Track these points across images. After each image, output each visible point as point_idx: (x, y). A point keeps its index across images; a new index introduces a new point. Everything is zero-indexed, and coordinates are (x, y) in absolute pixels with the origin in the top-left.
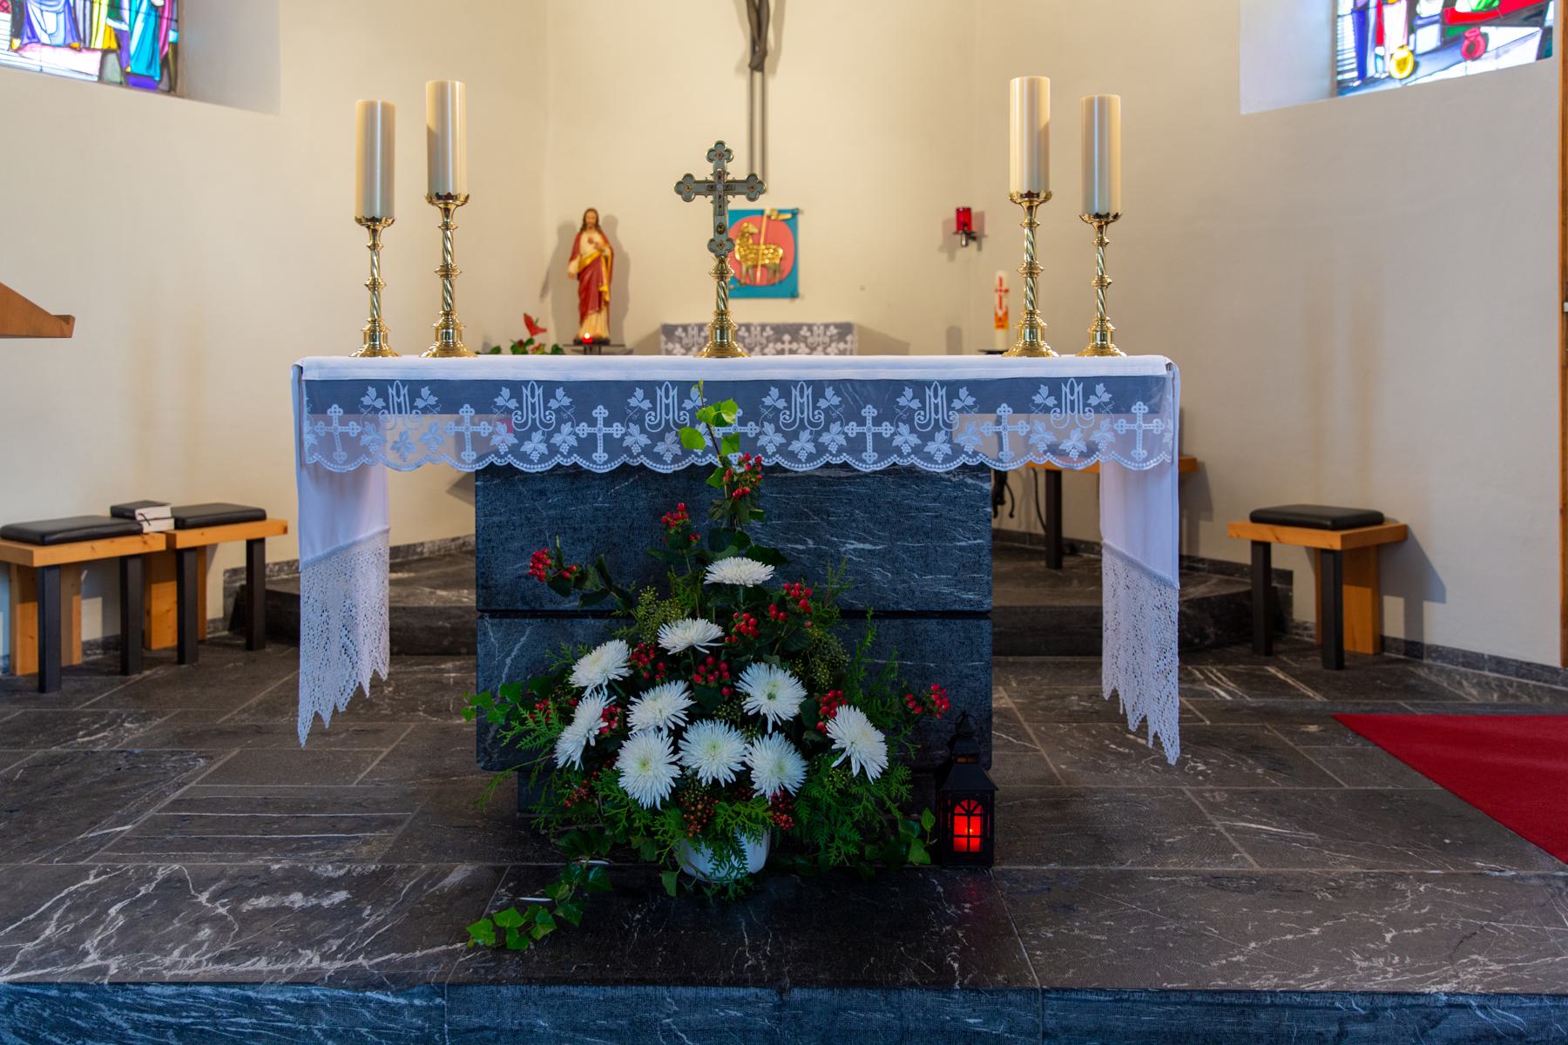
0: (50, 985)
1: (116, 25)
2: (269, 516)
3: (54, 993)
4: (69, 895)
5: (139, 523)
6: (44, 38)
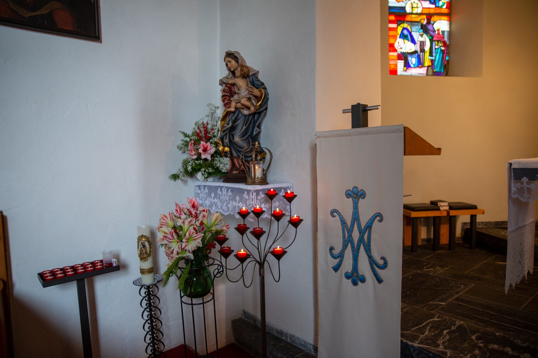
0: (430, 352)
1: (431, 58)
2: (478, 207)
3: (431, 355)
4: (430, 322)
5: (439, 207)
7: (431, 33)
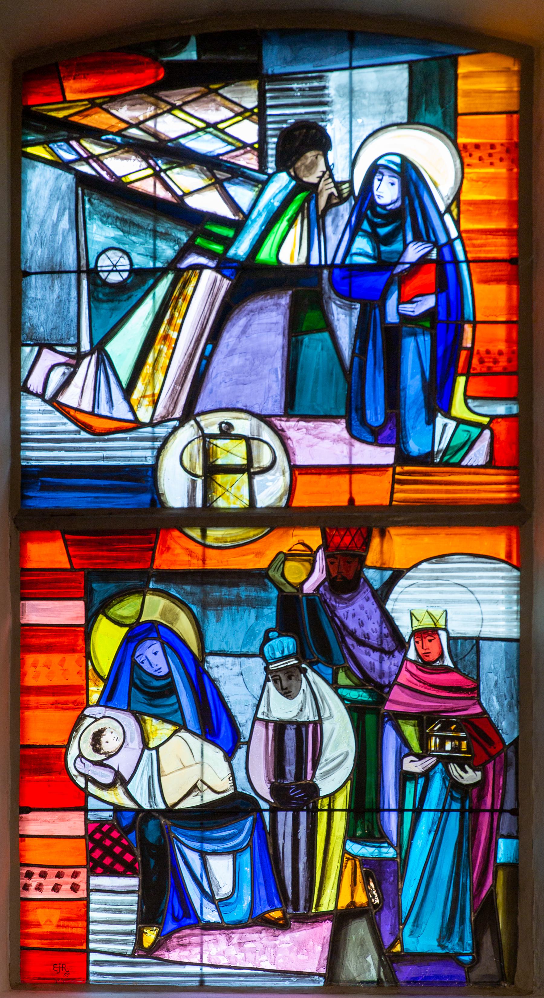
1: (367, 851)
6: (211, 915)
7: (369, 658)
